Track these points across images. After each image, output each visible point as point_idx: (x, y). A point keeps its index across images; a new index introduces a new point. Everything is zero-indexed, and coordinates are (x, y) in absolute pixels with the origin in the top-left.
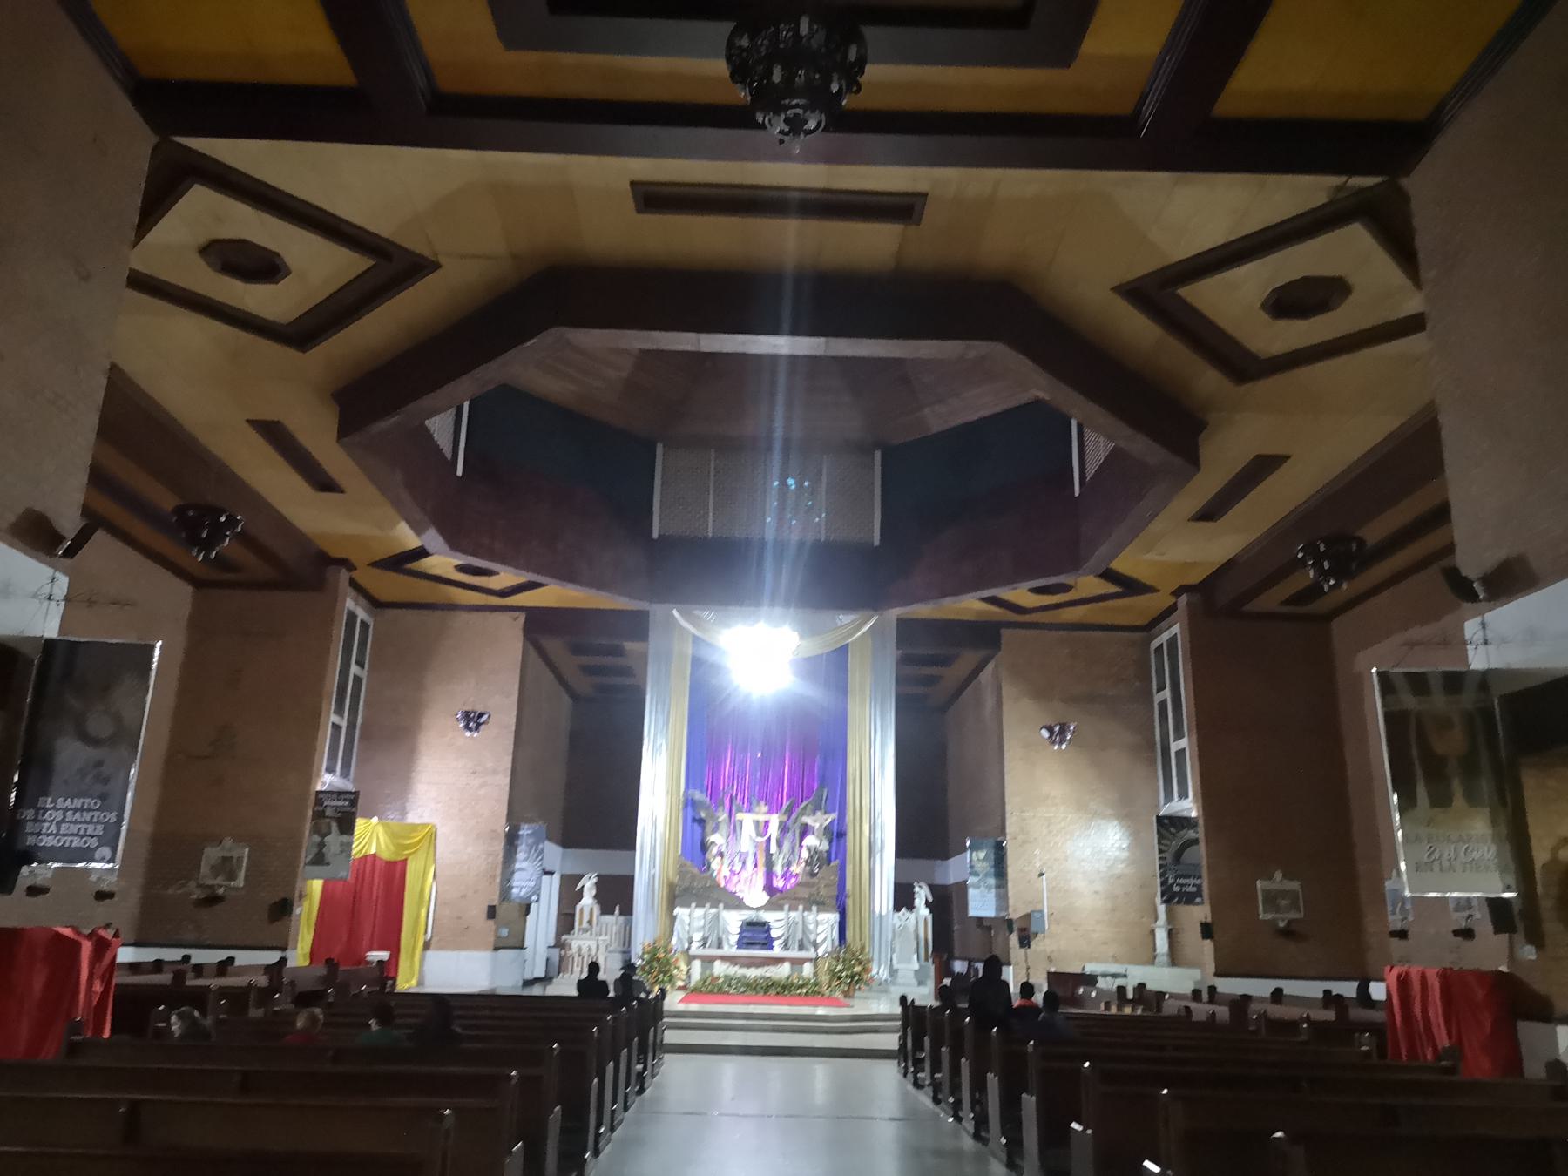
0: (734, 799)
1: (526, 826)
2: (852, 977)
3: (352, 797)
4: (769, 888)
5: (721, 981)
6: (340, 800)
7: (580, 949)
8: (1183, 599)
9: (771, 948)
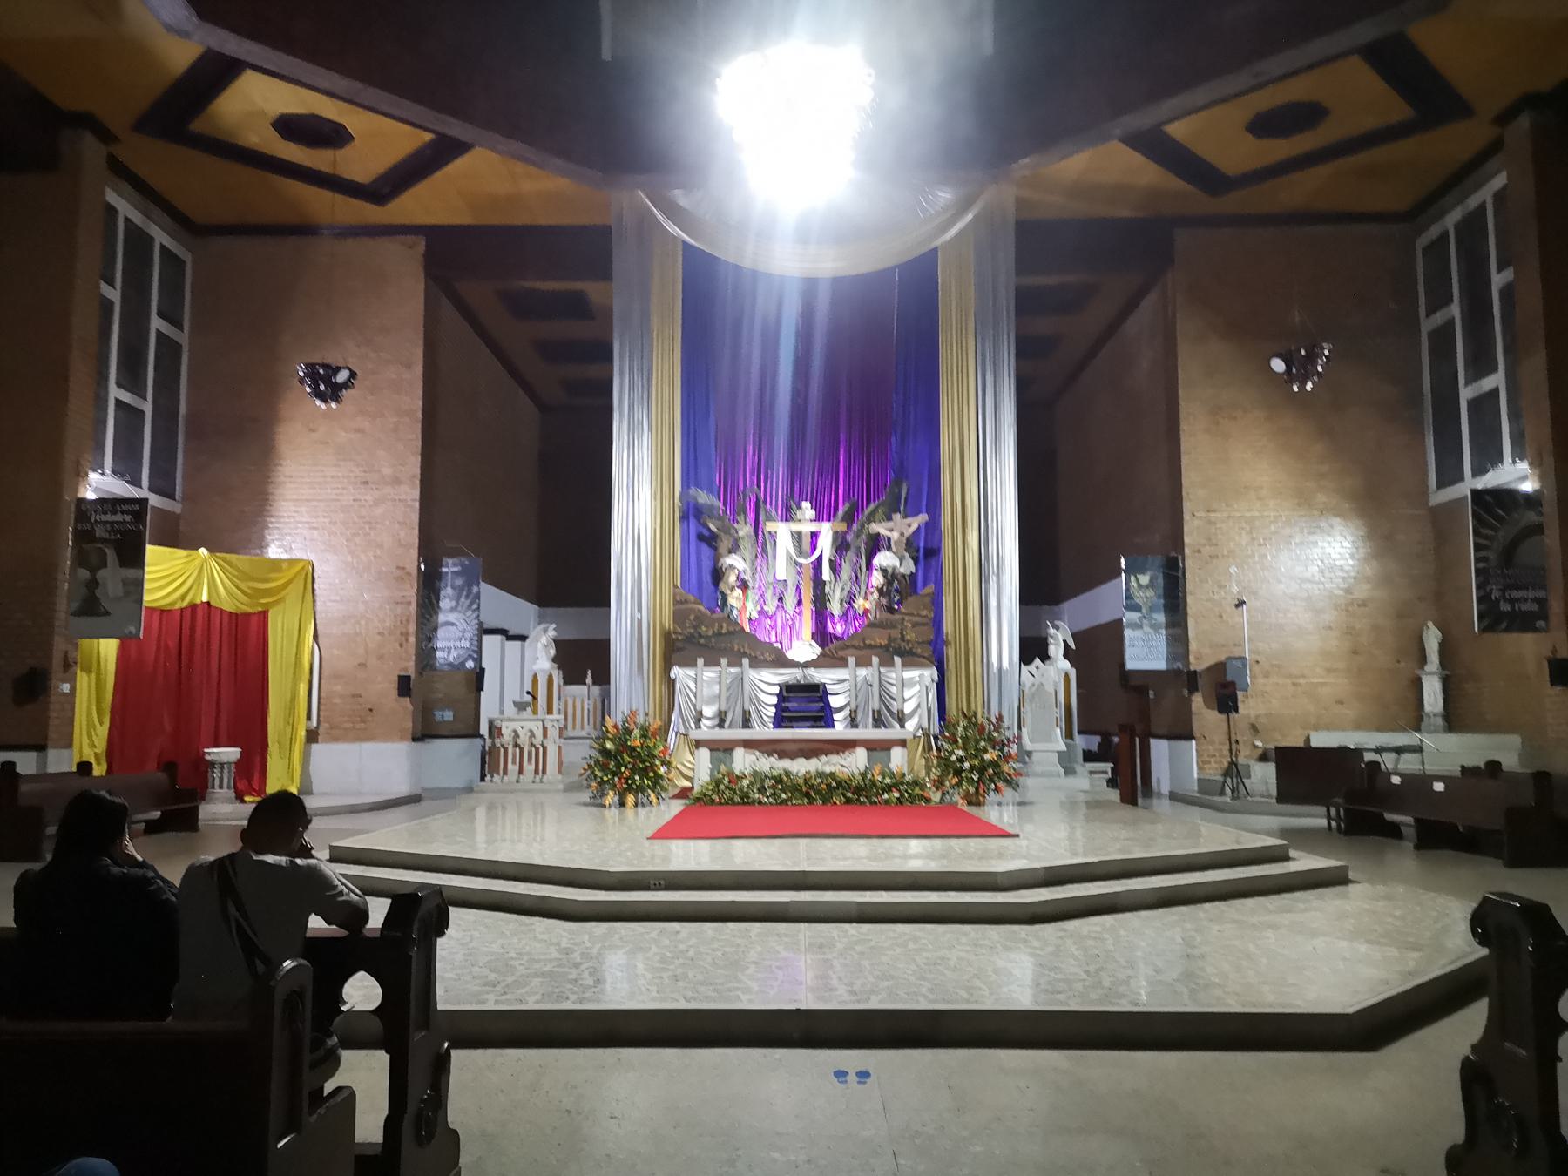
1: (450, 561)
2: (981, 770)
4: (821, 635)
5: (745, 782)
7: (516, 734)
8: (1524, 122)
9: (830, 724)
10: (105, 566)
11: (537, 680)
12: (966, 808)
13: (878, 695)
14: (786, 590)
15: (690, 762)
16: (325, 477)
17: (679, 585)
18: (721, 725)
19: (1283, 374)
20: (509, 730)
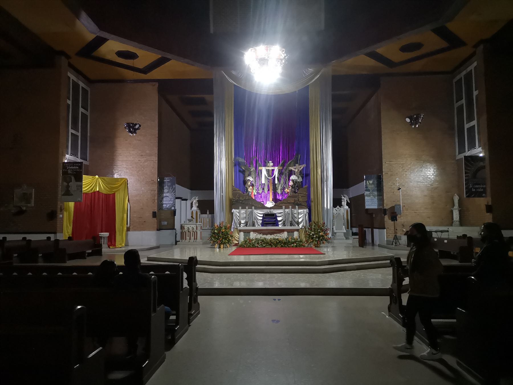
0: (257, 161)
3: (80, 165)
4: (275, 200)
7: (189, 229)
8: (482, 47)
9: (278, 225)
10: (71, 182)
11: (193, 213)
12: (314, 248)
13: (291, 217)
14: (265, 186)
15: (237, 236)
16: (130, 154)
17: (234, 185)
18: (246, 226)
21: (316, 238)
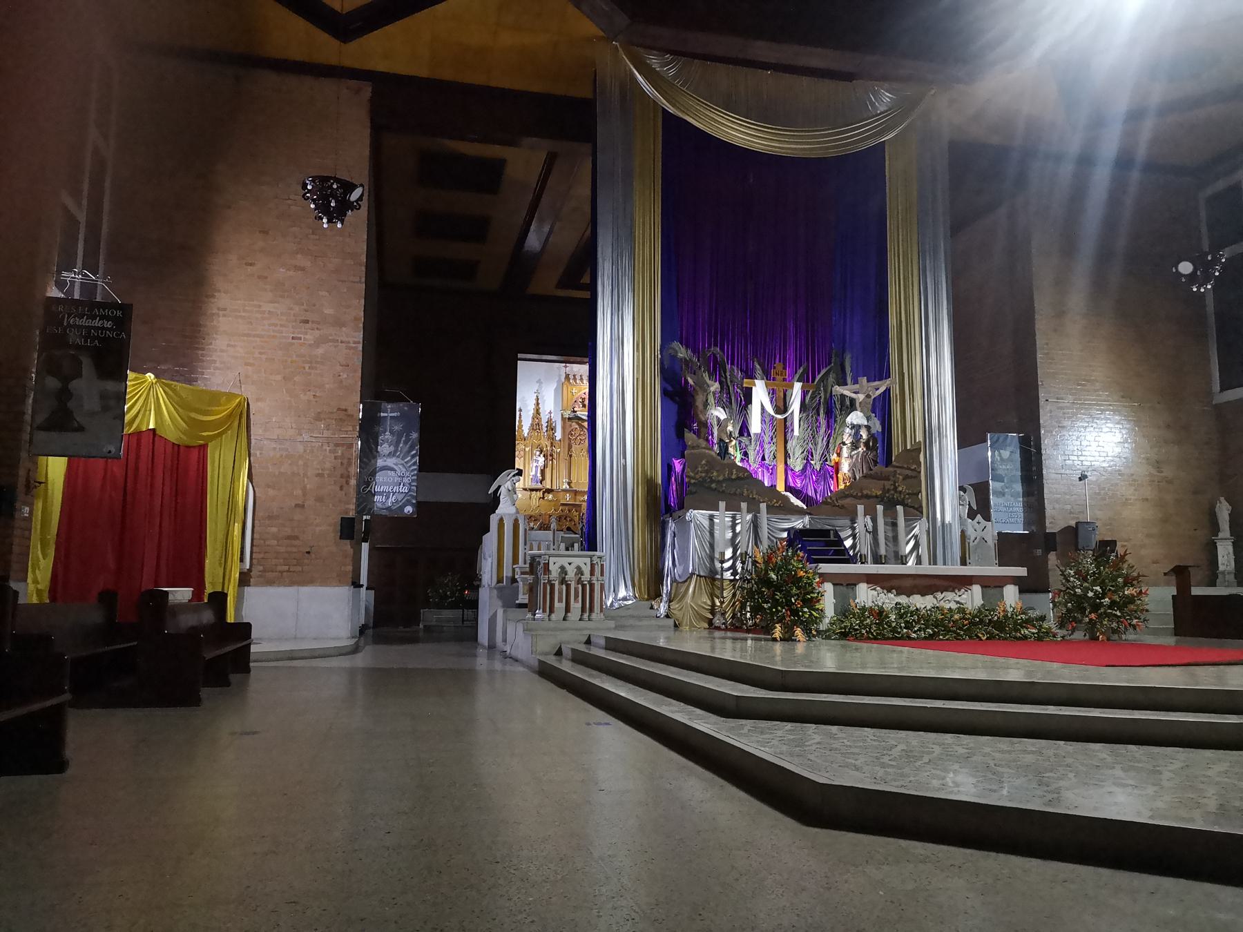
6: (94, 318)
19: (1184, 276)
20: (558, 565)
21: (1110, 607)
